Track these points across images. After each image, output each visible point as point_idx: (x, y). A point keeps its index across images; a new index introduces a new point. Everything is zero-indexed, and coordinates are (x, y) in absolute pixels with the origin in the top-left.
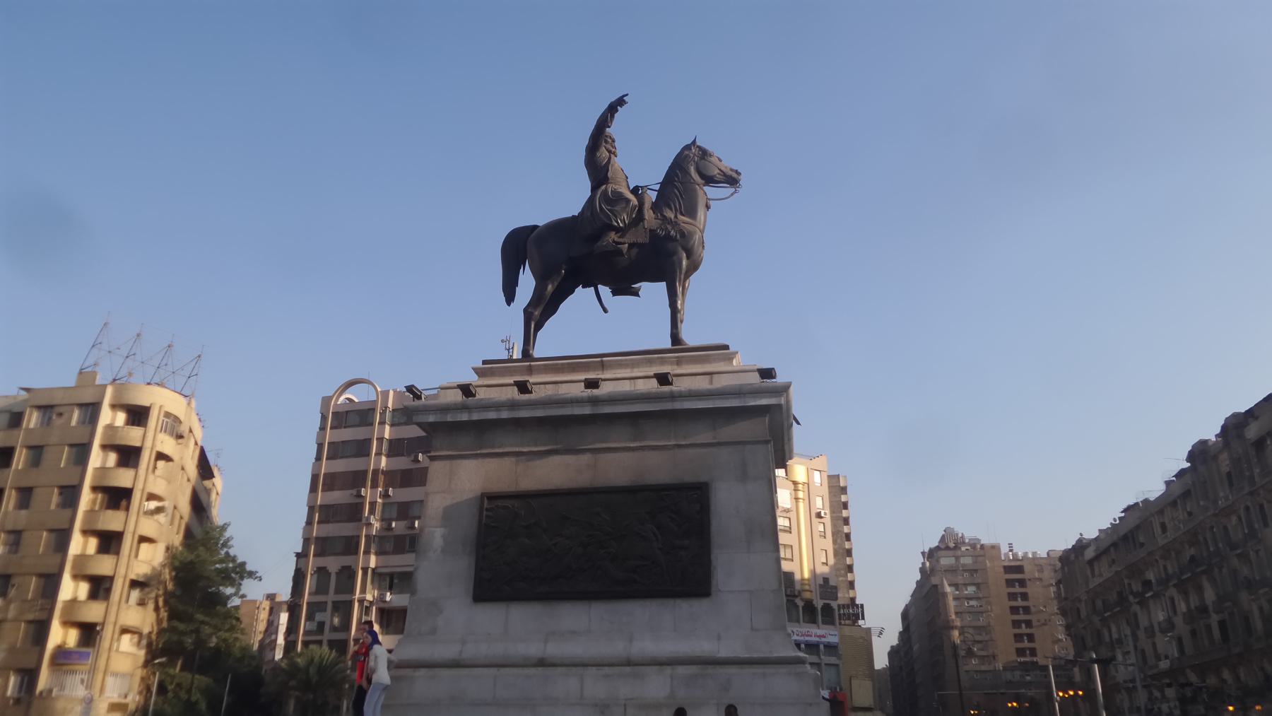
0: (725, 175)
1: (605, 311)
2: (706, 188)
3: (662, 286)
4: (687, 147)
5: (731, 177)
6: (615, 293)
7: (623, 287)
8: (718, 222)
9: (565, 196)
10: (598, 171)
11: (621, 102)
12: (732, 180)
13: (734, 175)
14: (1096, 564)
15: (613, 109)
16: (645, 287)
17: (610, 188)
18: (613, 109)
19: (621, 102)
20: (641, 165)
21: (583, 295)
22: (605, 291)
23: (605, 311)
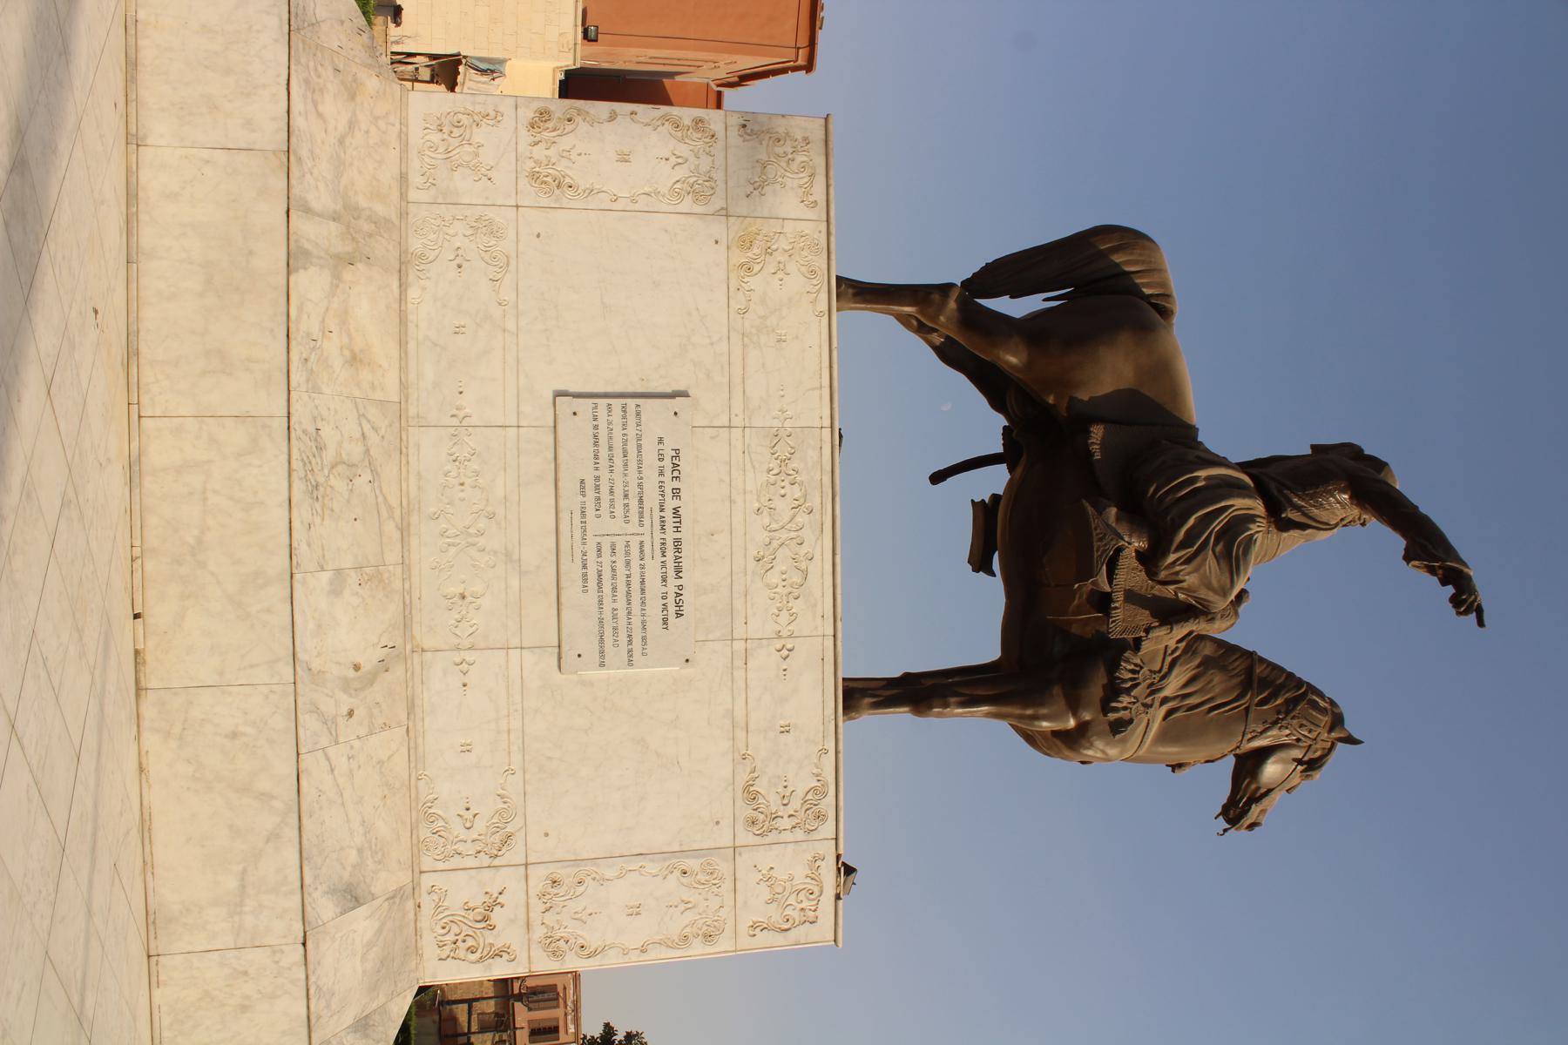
0: (1256, 799)
1: (937, 478)
2: (1230, 762)
3: (985, 647)
4: (1337, 721)
5: (1245, 811)
6: (985, 512)
7: (993, 533)
8: (1138, 792)
9: (1234, 405)
10: (1287, 486)
11: (1465, 599)
12: (1239, 807)
13: (1247, 821)
14: (348, 141)
15: (1426, 544)
16: (989, 596)
17: (1259, 530)
18: (1426, 544)
19: (1465, 599)
20: (1303, 595)
21: (985, 428)
22: (995, 480)
23: (937, 478)
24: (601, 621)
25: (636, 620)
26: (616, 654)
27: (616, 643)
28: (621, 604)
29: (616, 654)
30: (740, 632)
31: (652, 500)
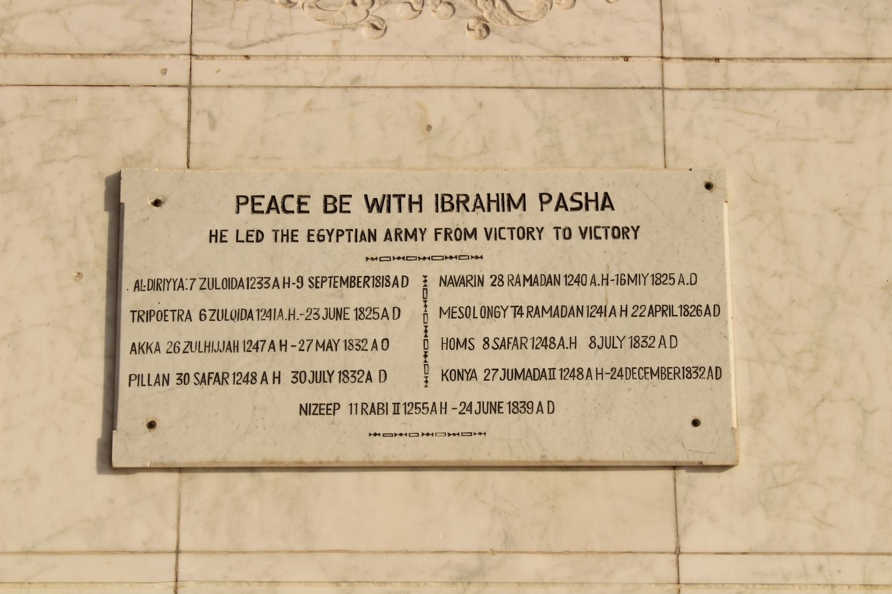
1: (237, 231)
23: (237, 231)
24: (617, 373)
25: (617, 296)
26: (693, 342)
27: (670, 342)
28: (580, 328)
29: (693, 342)
30: (645, 72)
31: (349, 258)
